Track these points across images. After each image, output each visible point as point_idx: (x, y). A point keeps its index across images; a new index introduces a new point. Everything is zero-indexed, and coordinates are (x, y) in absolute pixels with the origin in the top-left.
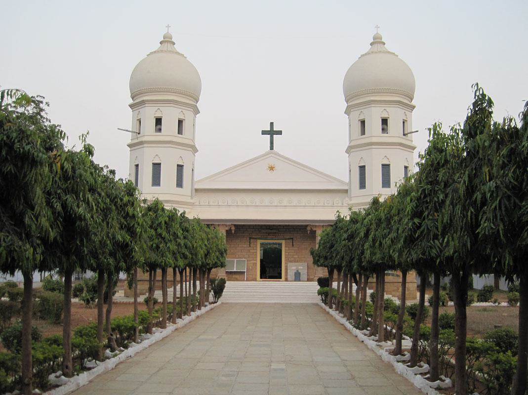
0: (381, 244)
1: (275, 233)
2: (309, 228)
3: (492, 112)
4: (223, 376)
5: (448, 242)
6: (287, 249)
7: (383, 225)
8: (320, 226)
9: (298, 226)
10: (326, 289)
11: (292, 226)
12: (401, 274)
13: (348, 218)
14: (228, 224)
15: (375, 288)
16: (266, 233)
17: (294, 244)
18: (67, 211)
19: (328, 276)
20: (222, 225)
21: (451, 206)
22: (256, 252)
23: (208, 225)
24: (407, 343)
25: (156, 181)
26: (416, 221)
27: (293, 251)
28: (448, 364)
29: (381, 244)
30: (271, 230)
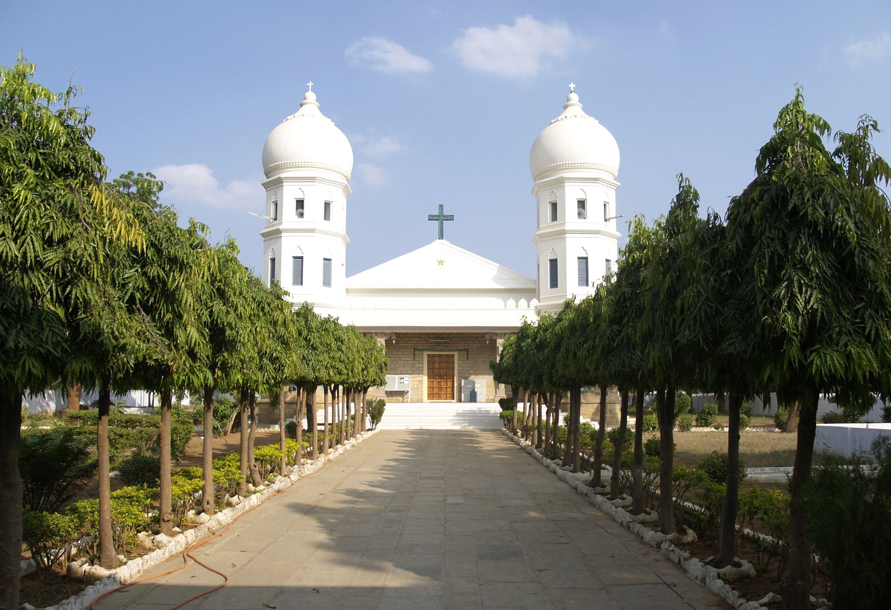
0: (575, 355)
1: (447, 343)
2: (488, 337)
3: (698, 206)
4: (390, 511)
5: (649, 352)
6: (461, 362)
7: (578, 333)
8: (501, 333)
9: (475, 334)
10: (508, 412)
11: (468, 334)
12: (599, 391)
13: (536, 325)
14: (387, 331)
15: (569, 410)
16: (435, 343)
17: (469, 356)
18: (214, 319)
19: (512, 397)
20: (381, 333)
21: (651, 311)
22: (422, 367)
23: (365, 334)
24: (607, 473)
25: (299, 279)
26: (615, 327)
27: (468, 365)
28: (653, 495)
29: (575, 355)
30: (442, 339)
